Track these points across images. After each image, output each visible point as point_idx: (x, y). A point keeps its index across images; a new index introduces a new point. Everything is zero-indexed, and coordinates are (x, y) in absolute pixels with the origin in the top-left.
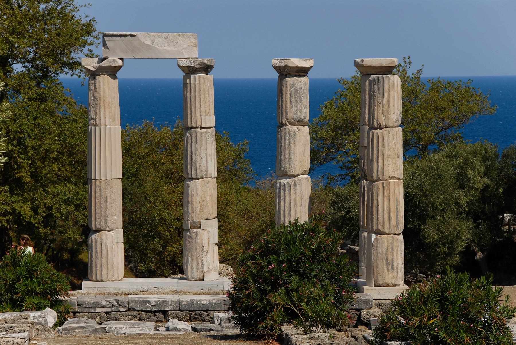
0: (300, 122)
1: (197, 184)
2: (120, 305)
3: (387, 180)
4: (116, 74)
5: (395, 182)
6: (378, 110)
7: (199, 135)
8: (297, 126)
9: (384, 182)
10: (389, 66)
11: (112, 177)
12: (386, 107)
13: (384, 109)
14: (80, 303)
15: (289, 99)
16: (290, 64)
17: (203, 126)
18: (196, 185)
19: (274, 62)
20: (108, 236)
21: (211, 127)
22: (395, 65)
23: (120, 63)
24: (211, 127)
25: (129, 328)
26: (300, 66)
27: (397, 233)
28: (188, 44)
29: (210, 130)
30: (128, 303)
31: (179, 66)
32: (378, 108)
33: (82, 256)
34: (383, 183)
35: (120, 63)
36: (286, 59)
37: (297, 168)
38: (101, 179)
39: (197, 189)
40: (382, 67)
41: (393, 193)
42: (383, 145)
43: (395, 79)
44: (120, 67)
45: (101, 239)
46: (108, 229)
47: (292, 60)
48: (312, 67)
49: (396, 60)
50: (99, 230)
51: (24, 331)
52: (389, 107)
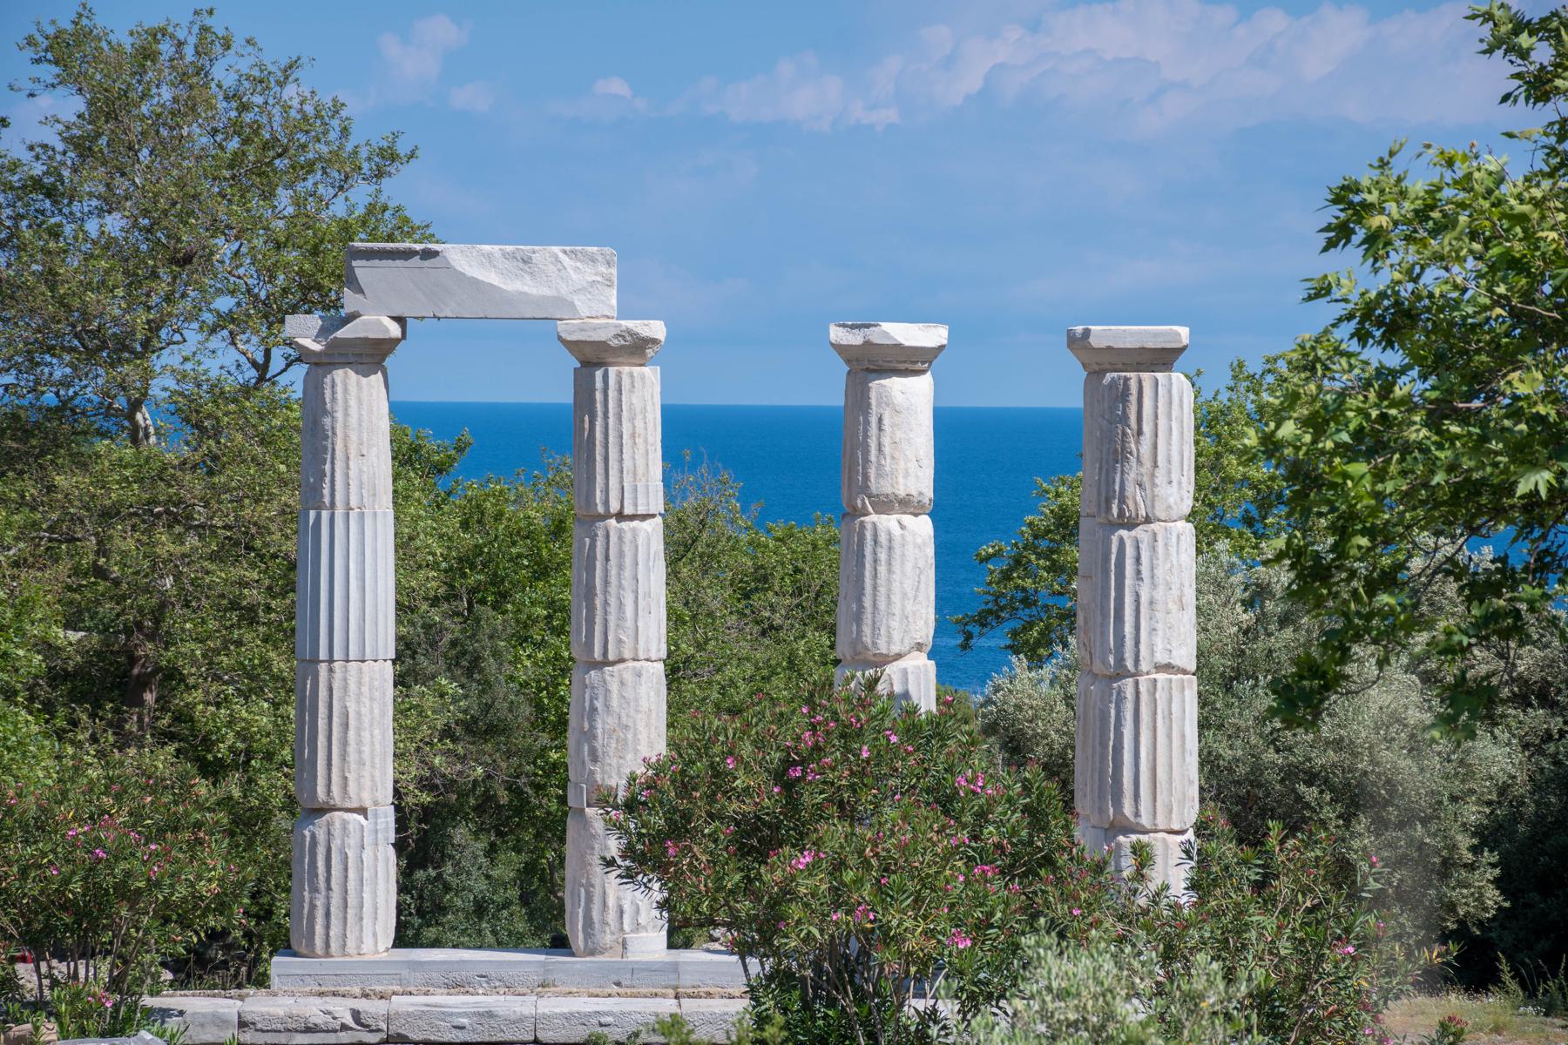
0: (906, 505)
1: (608, 678)
2: (362, 1025)
3: (1148, 673)
4: (384, 360)
5: (1170, 681)
6: (1123, 472)
7: (613, 539)
8: (898, 516)
9: (1141, 679)
10: (1164, 349)
11: (364, 655)
12: (1148, 463)
13: (1143, 470)
14: (248, 1018)
15: (874, 438)
16: (877, 340)
17: (628, 511)
18: (604, 681)
19: (837, 334)
20: (351, 827)
21: (653, 516)
22: (1180, 346)
23: (394, 330)
24: (653, 516)
25: (591, 995)
26: (907, 343)
27: (1176, 827)
28: (589, 279)
29: (647, 525)
30: (388, 1019)
31: (560, 338)
32: (1122, 466)
33: (404, 863)
34: (1137, 683)
35: (394, 330)
36: (868, 326)
37: (896, 636)
38: (348, 661)
39: (607, 691)
40: (1143, 350)
41: (1166, 713)
42: (1139, 572)
43: (1177, 383)
44: (394, 342)
45: (329, 833)
46: (348, 805)
47: (886, 326)
48: (942, 347)
49: (1184, 332)
50: (325, 807)
51: (382, 997)
52: (1155, 465)
